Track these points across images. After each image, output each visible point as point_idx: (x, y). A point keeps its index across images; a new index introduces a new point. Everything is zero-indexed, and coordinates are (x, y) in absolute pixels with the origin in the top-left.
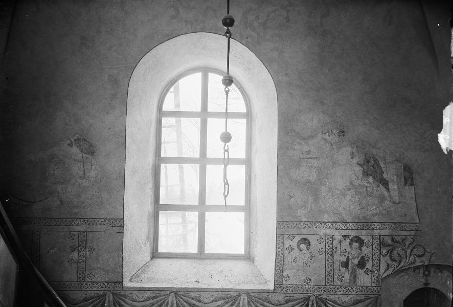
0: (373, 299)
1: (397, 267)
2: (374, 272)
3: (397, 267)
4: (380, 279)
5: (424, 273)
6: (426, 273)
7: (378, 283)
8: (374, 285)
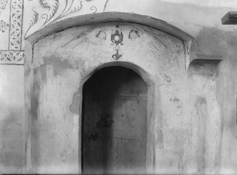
0: (29, 141)
1: (51, 18)
2: (13, 27)
3: (51, 18)
4: (23, 39)
5: (113, 37)
6: (117, 38)
7: (18, 45)
8: (13, 48)
